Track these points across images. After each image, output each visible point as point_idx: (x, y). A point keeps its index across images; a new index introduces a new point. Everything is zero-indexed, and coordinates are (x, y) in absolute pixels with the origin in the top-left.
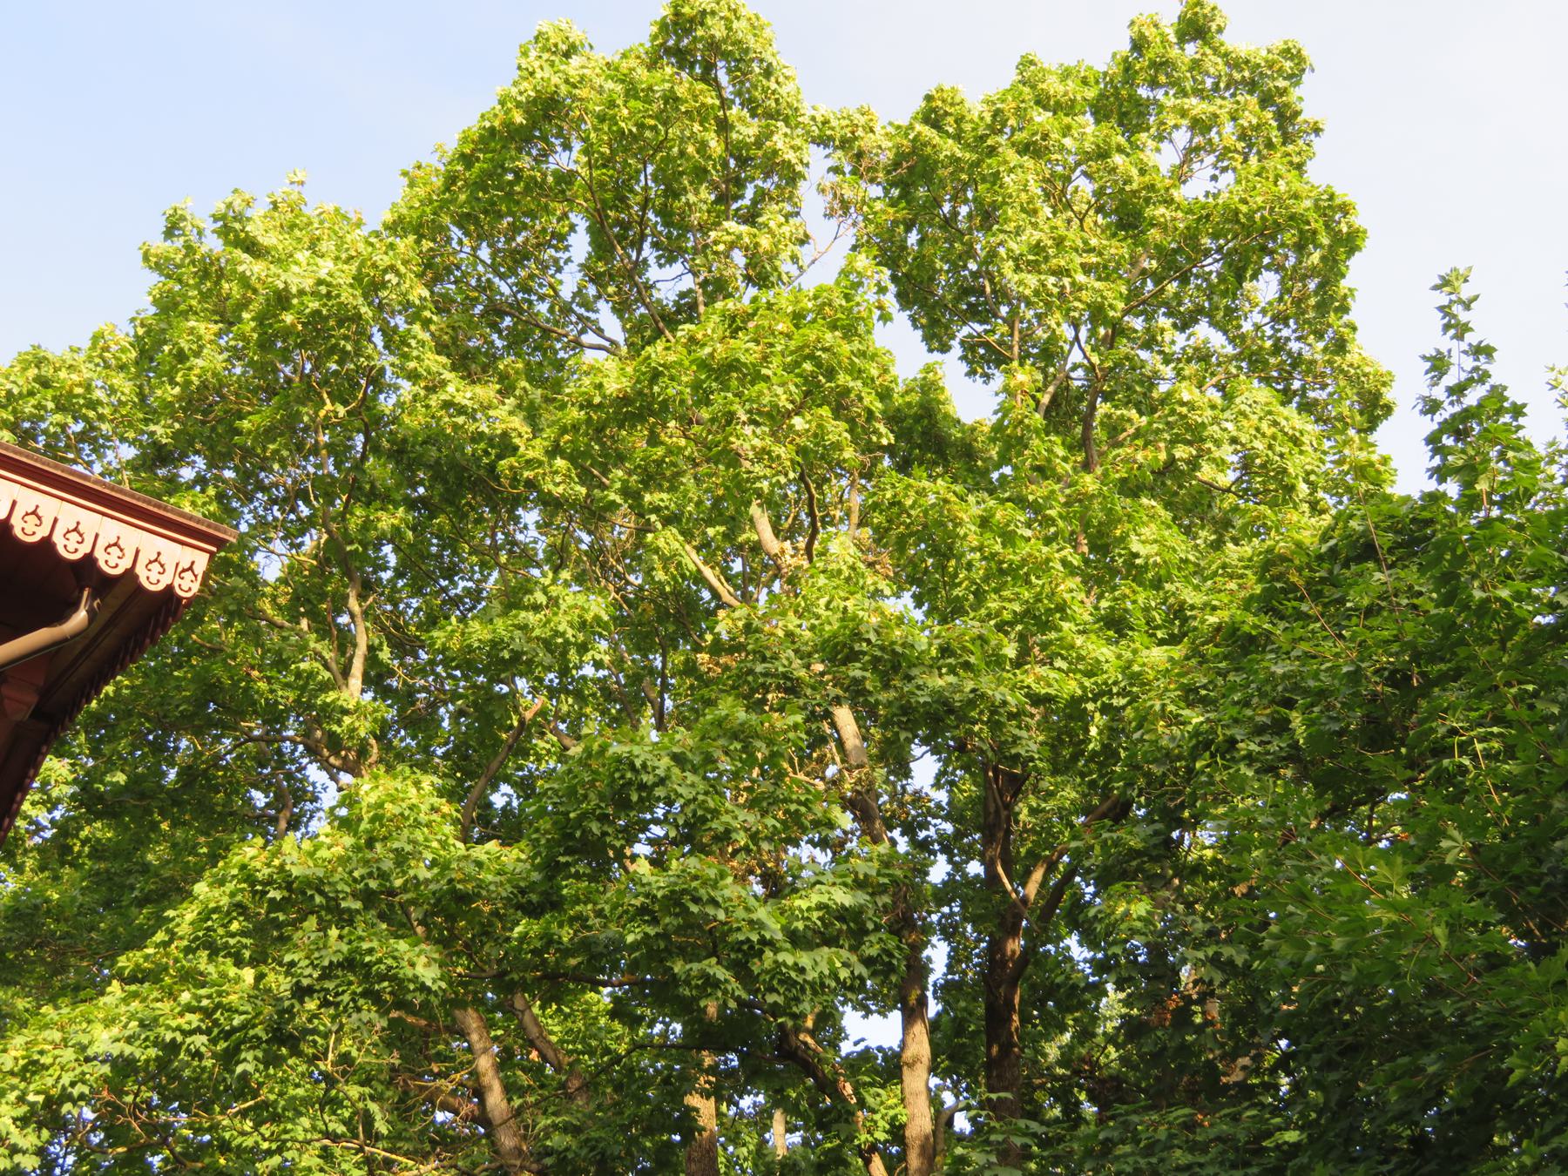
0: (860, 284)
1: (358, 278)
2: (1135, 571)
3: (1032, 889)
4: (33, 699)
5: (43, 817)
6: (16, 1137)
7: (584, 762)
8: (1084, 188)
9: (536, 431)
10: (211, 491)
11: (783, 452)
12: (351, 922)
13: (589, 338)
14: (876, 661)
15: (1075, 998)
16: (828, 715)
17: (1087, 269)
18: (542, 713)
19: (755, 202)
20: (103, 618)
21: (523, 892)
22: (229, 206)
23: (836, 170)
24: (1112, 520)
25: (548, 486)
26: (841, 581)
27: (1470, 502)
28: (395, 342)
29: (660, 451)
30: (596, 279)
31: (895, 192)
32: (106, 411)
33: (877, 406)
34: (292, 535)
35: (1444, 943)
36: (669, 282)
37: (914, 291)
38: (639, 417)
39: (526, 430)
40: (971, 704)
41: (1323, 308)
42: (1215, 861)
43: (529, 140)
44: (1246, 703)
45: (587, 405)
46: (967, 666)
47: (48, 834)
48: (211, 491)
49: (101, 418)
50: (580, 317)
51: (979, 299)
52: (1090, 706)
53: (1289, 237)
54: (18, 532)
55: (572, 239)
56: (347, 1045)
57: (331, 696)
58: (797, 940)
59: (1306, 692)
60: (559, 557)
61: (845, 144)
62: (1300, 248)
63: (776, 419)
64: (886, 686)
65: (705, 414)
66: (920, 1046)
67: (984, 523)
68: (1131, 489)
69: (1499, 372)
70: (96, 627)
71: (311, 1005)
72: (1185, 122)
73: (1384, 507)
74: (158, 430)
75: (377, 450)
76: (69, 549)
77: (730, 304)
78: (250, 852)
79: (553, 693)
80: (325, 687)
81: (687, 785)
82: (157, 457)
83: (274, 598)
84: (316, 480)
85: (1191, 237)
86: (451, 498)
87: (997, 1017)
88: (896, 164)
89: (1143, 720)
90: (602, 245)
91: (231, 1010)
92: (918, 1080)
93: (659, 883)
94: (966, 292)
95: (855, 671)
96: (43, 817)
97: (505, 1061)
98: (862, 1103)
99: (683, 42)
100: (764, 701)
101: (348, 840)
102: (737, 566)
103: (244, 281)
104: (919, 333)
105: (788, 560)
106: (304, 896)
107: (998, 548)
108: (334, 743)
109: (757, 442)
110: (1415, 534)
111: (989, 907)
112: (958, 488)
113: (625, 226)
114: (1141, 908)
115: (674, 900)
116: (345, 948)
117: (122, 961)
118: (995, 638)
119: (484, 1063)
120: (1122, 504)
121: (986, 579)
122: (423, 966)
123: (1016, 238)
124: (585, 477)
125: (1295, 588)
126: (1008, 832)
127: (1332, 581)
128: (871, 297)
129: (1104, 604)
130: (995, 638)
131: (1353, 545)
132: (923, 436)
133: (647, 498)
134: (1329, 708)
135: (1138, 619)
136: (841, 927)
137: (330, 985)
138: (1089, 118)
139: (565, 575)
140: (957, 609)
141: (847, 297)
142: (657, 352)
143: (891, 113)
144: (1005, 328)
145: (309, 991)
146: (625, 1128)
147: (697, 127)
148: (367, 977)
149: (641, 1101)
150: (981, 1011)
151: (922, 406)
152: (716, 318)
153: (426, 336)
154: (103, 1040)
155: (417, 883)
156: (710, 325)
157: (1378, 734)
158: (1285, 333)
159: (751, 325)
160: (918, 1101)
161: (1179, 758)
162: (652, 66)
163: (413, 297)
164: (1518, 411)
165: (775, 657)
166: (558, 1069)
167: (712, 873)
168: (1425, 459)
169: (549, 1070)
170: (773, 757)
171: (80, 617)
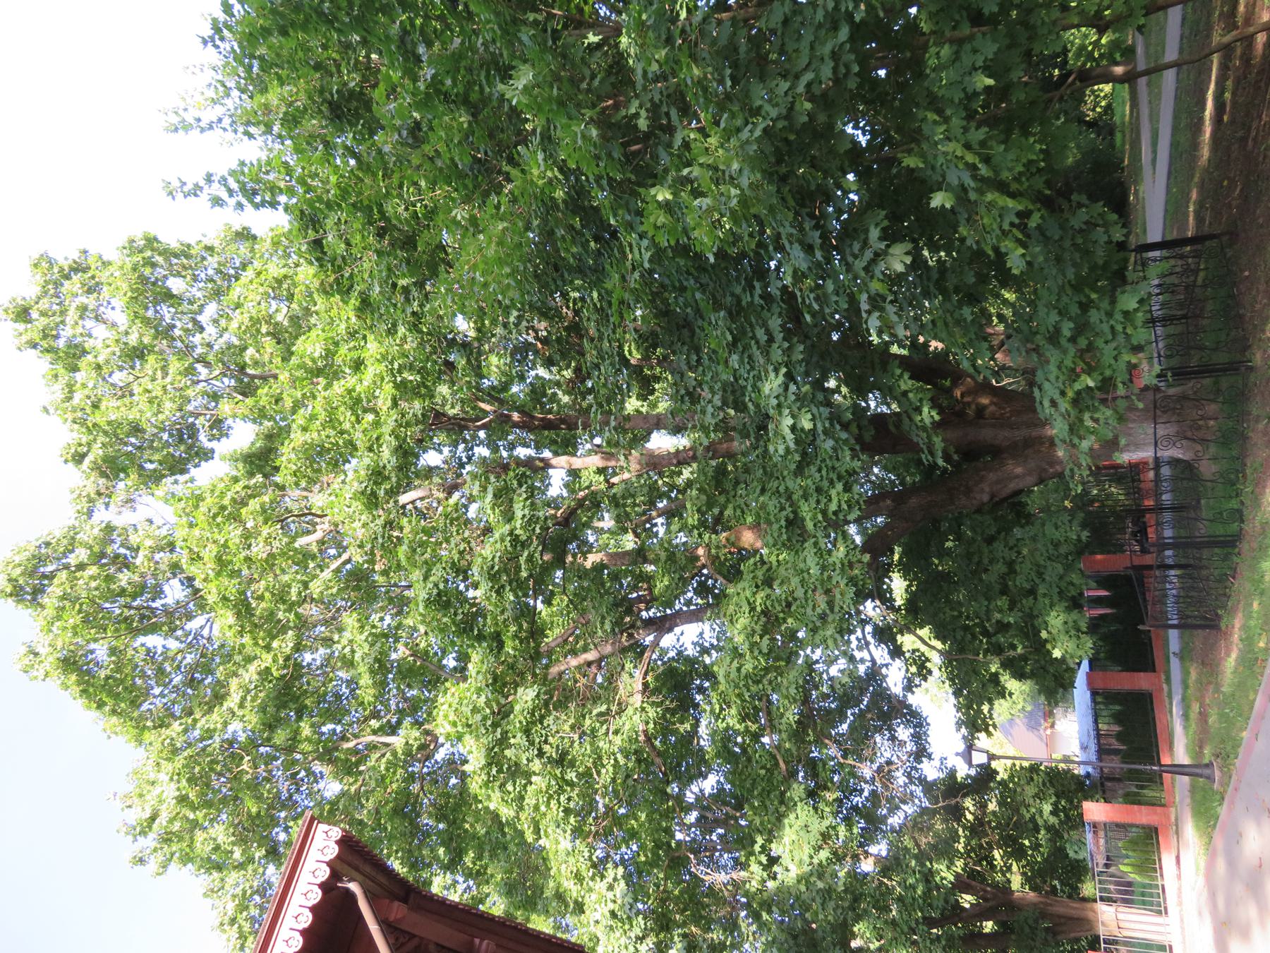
0: (173, 494)
1: (168, 759)
2: (329, 354)
3: (488, 407)
4: (396, 904)
5: (460, 888)
6: (610, 879)
7: (428, 624)
8: (119, 377)
9: (255, 658)
10: (291, 824)
11: (265, 531)
12: (507, 732)
13: (206, 632)
14: (375, 483)
15: (538, 391)
16: (404, 507)
17: (165, 374)
18: (406, 645)
19: (128, 548)
20: (354, 874)
21: (492, 650)
22: (127, 833)
23: (107, 505)
24: (302, 366)
25: (288, 651)
26: (338, 501)
27: (291, 191)
28: (209, 734)
29: (267, 595)
30: (173, 630)
31: (122, 475)
32: (248, 885)
33: (241, 484)
34: (317, 777)
35: (505, 224)
36: (174, 592)
37: (177, 467)
38: (248, 606)
39: (256, 663)
40: (397, 437)
41: (188, 256)
42: (475, 322)
43: (89, 672)
44: (395, 305)
45: (241, 633)
46: (378, 439)
47: (471, 883)
48: (291, 824)
49: (251, 887)
50: (195, 638)
51: (185, 434)
52: (399, 379)
53: (147, 271)
54: (306, 925)
55: (150, 645)
56: (566, 728)
57: (400, 751)
58: (509, 517)
59: (389, 277)
60: (328, 642)
61: (91, 501)
62: (154, 265)
63: (247, 536)
64: (389, 478)
65: (245, 572)
66: (562, 460)
67: (305, 429)
68: (287, 355)
69: (221, 170)
70: (360, 877)
71: (546, 748)
72: (80, 322)
73: (294, 233)
74: (257, 855)
75: (269, 739)
76: (316, 896)
77: (183, 561)
78: (475, 786)
79: (397, 640)
80: (394, 754)
81: (437, 573)
82: (273, 853)
83: (351, 784)
84: (286, 770)
85: (147, 322)
86: (296, 699)
87: (548, 425)
88: (107, 477)
89: (404, 355)
90: (153, 629)
91: (549, 786)
92: (577, 463)
93: (484, 587)
94: (181, 440)
95: (381, 493)
96: (460, 888)
97: (574, 652)
98: (588, 487)
99: (29, 587)
100: (398, 538)
101: (467, 737)
102: (332, 552)
103: (171, 821)
104: (203, 463)
105: (326, 527)
106: (494, 759)
107: (318, 423)
108: (423, 747)
109: (261, 545)
110: (309, 220)
111: (499, 426)
112: (286, 442)
113: (142, 617)
114: (494, 359)
115: (493, 577)
116: (519, 735)
117: (530, 840)
118: (364, 425)
119: (574, 662)
120: (294, 360)
121: (334, 428)
122: (526, 696)
123: (140, 411)
124: (284, 630)
125: (337, 279)
126: (462, 419)
127: (333, 261)
128: (180, 487)
129: (347, 371)
130: (364, 425)
131: (315, 250)
132: (260, 461)
133: (294, 598)
134: (396, 266)
135: (355, 354)
136: (503, 497)
137: (537, 740)
138: (77, 374)
139: (336, 637)
140: (352, 445)
141: (180, 500)
142: (212, 598)
143: (81, 479)
144: (202, 418)
145: (540, 750)
146: (602, 597)
147: (81, 582)
148: (534, 723)
149: (589, 589)
150: (546, 433)
151: (245, 462)
152: (192, 568)
153: (204, 720)
154: (565, 844)
155: (488, 703)
156: (193, 570)
157: (409, 242)
158: (203, 276)
159: (196, 550)
160: (587, 461)
161: (422, 339)
162: (43, 607)
163: (180, 729)
164: (242, 164)
165: (375, 533)
166: (577, 627)
167: (480, 560)
168: (266, 212)
169: (578, 632)
170: (424, 531)
171: (354, 887)
